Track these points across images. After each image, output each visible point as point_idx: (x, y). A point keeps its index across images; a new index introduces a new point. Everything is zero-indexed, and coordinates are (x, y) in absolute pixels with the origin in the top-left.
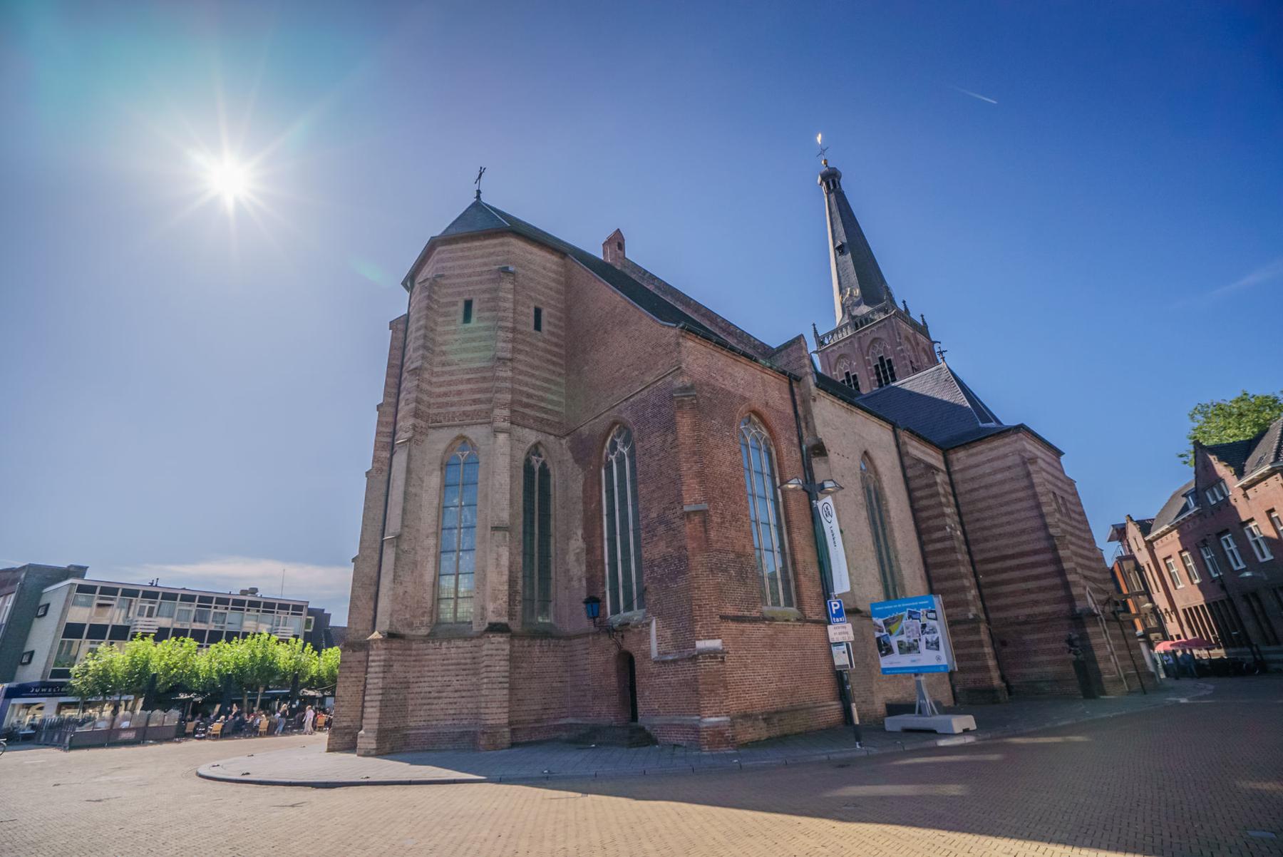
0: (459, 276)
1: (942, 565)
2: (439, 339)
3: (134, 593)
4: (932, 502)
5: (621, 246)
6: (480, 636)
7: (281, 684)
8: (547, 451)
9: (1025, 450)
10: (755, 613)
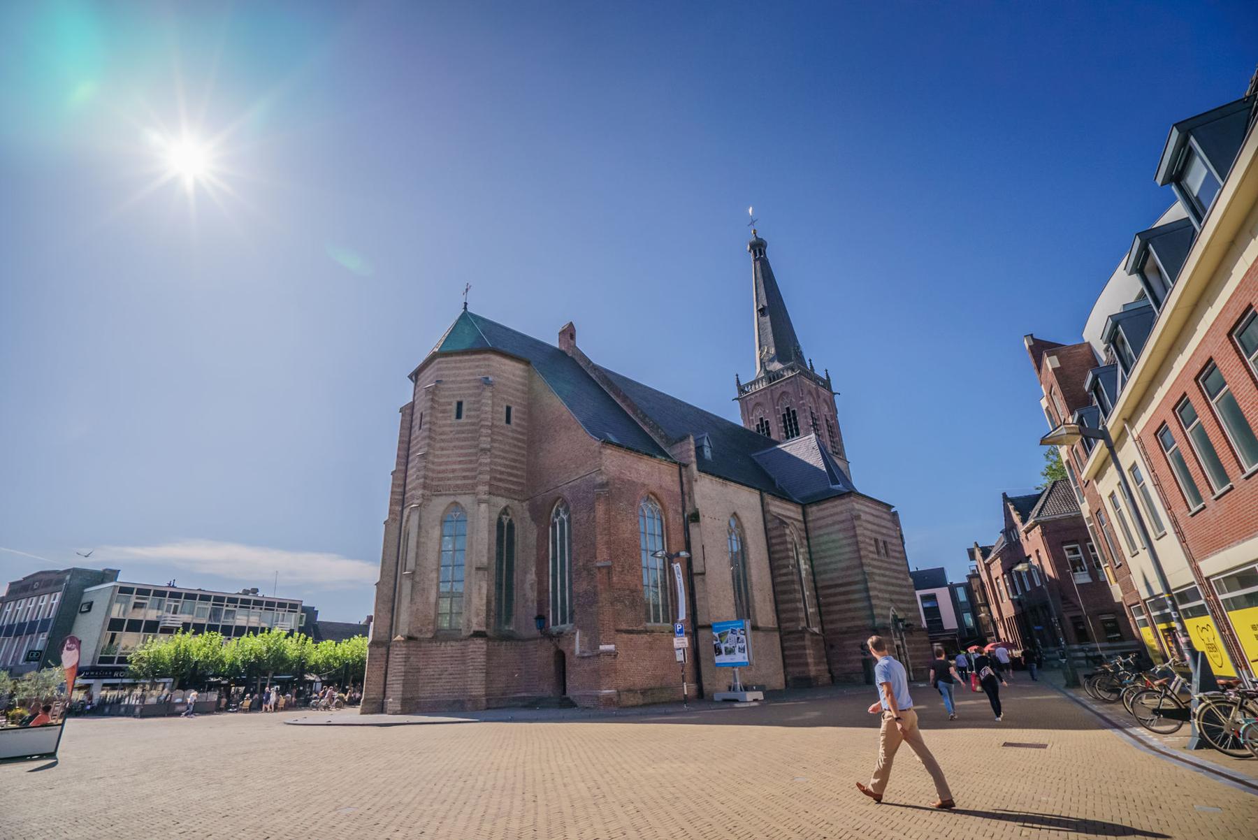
0: (453, 382)
1: (785, 592)
2: (438, 437)
3: (163, 594)
4: (782, 547)
5: (572, 337)
6: (466, 639)
7: (288, 670)
9: (853, 509)
10: (641, 628)
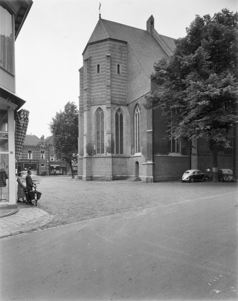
8: (122, 111)
